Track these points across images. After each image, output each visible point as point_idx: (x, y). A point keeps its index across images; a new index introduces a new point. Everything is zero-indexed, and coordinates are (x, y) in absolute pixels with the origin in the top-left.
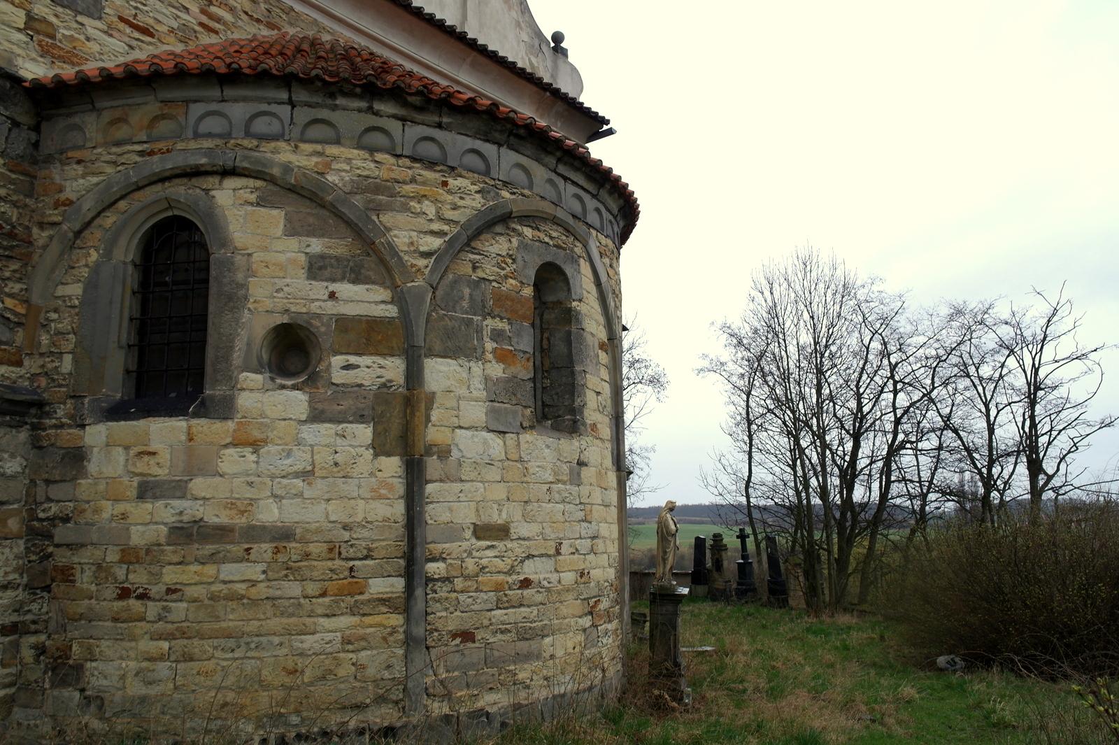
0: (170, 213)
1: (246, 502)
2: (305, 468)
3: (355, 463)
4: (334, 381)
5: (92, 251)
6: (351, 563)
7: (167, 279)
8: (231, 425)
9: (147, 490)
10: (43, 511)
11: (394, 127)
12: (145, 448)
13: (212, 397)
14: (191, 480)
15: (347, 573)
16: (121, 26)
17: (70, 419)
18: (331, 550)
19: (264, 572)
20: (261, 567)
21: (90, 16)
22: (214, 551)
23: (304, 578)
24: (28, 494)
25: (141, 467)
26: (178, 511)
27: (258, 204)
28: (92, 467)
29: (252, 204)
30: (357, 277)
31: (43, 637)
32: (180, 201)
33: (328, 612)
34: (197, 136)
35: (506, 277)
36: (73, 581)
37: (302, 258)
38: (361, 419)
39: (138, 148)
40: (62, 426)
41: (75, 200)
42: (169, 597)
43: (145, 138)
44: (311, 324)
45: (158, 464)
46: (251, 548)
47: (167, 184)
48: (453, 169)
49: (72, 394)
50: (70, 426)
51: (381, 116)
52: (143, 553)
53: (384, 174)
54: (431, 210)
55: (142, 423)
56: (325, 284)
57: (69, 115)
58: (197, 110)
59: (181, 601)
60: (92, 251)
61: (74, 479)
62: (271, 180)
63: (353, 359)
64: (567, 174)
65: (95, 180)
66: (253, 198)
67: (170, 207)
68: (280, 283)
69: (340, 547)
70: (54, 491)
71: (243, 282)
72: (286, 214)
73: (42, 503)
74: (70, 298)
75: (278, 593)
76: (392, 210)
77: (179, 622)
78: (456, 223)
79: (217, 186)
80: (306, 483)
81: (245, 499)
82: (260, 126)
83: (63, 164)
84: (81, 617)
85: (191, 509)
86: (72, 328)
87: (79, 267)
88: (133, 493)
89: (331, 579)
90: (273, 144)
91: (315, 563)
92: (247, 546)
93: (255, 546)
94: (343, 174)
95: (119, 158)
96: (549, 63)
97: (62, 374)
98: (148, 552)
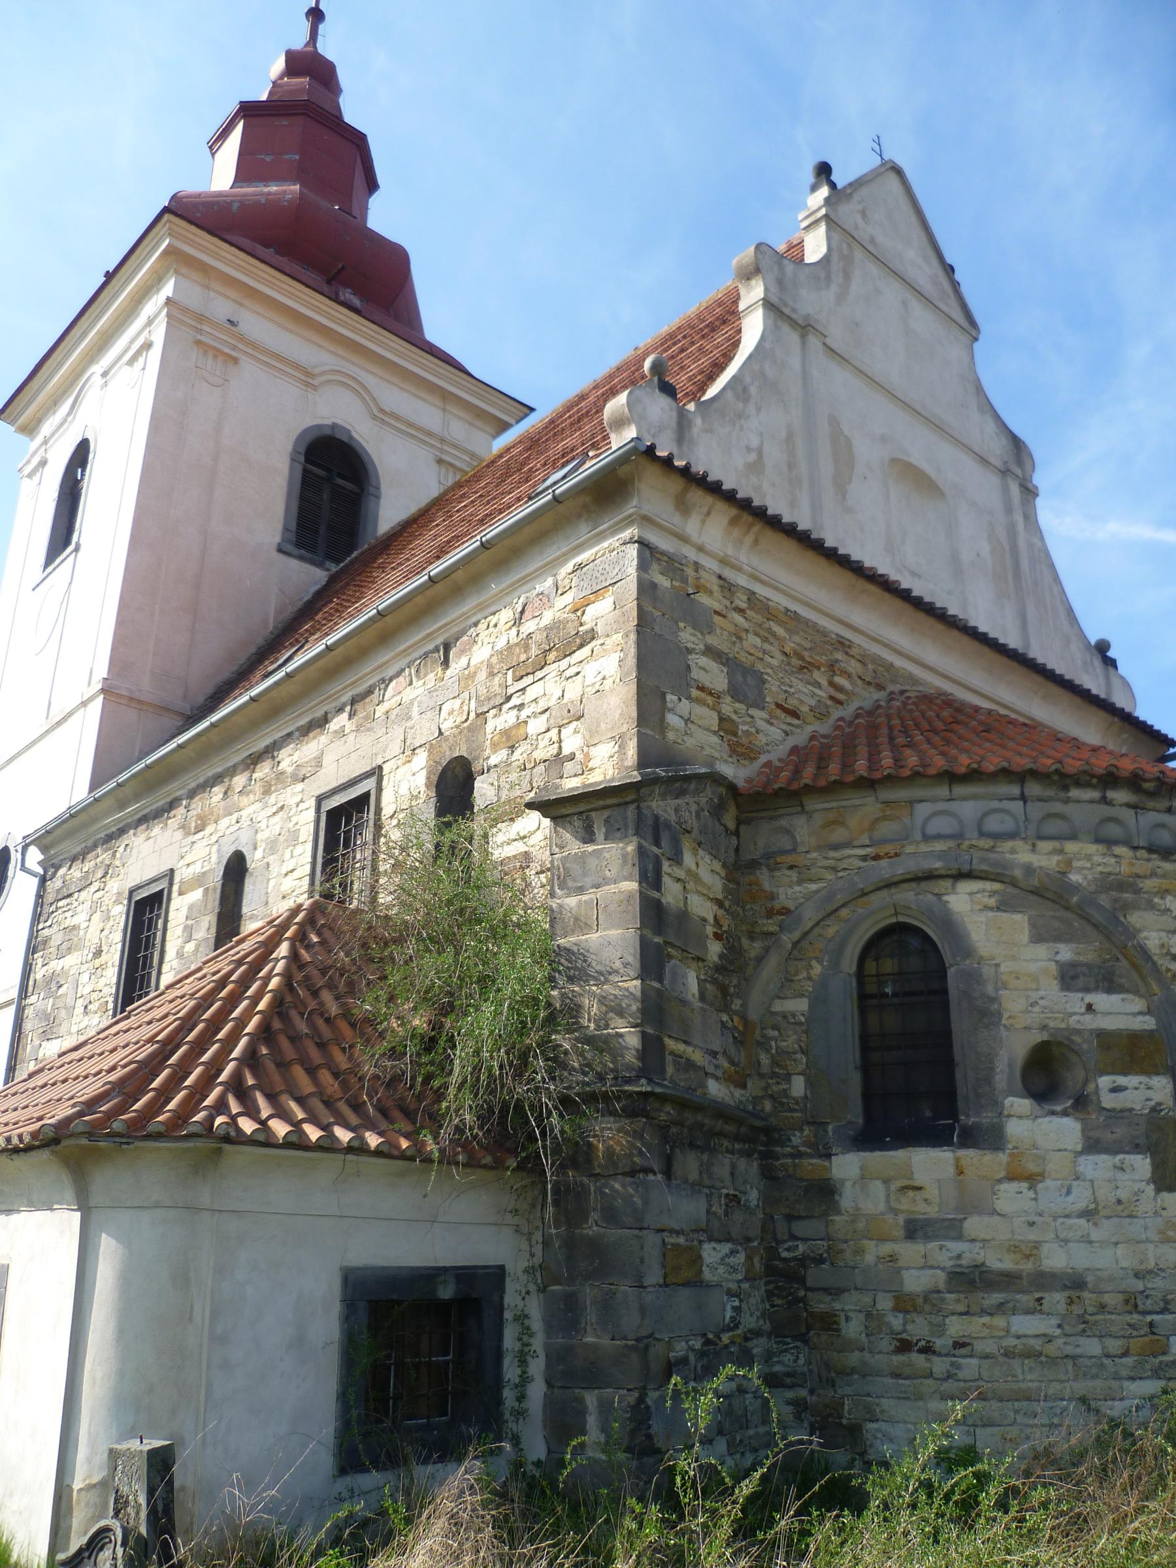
0: (894, 920)
1: (1030, 1245)
2: (1087, 1206)
3: (1138, 1200)
4: (1104, 1105)
5: (814, 963)
6: (1149, 1318)
7: (887, 990)
8: (1003, 1157)
9: (915, 1230)
10: (788, 1250)
11: (1128, 815)
12: (908, 1183)
13: (977, 1126)
14: (965, 1218)
15: (1146, 1329)
16: (778, 712)
17: (809, 1148)
18: (1127, 1302)
19: (1059, 1326)
20: (1054, 1321)
22: (1002, 1301)
23: (1103, 1333)
24: (763, 1230)
25: (905, 1203)
26: (954, 1254)
27: (998, 909)
28: (846, 1201)
29: (991, 909)
30: (1110, 984)
31: (803, 1393)
32: (910, 908)
33: (1132, 1374)
34: (927, 838)
36: (838, 1330)
37: (1053, 967)
38: (1136, 1149)
40: (800, 1155)
41: (792, 909)
42: (957, 1352)
43: (867, 842)
44: (1072, 1042)
45: (926, 1200)
46: (1042, 1298)
47: (893, 890)
49: (811, 1120)
50: (811, 1156)
51: (1114, 805)
52: (920, 1301)
53: (1125, 869)
55: (900, 1154)
56: (1080, 995)
58: (922, 810)
59: (971, 1356)
60: (814, 963)
61: (826, 1214)
62: (1013, 883)
63: (1121, 1080)
66: (992, 902)
67: (896, 914)
68: (1034, 996)
69: (1135, 1298)
70: (800, 1228)
71: (994, 995)
72: (1029, 919)
73: (784, 1241)
74: (793, 1015)
75: (1079, 1351)
76: (1139, 909)
77: (971, 1381)
79: (950, 890)
80: (1090, 1223)
81: (1029, 1242)
82: (993, 824)
83: (771, 869)
84: (853, 1371)
85: (971, 1254)
86: (800, 1046)
87: (799, 981)
88: (900, 1233)
89: (1130, 1336)
91: (1113, 1317)
92: (1037, 1295)
93: (1045, 1295)
94: (1086, 872)
95: (839, 863)
96: (1102, 681)
97: (794, 1098)
98: (926, 1299)
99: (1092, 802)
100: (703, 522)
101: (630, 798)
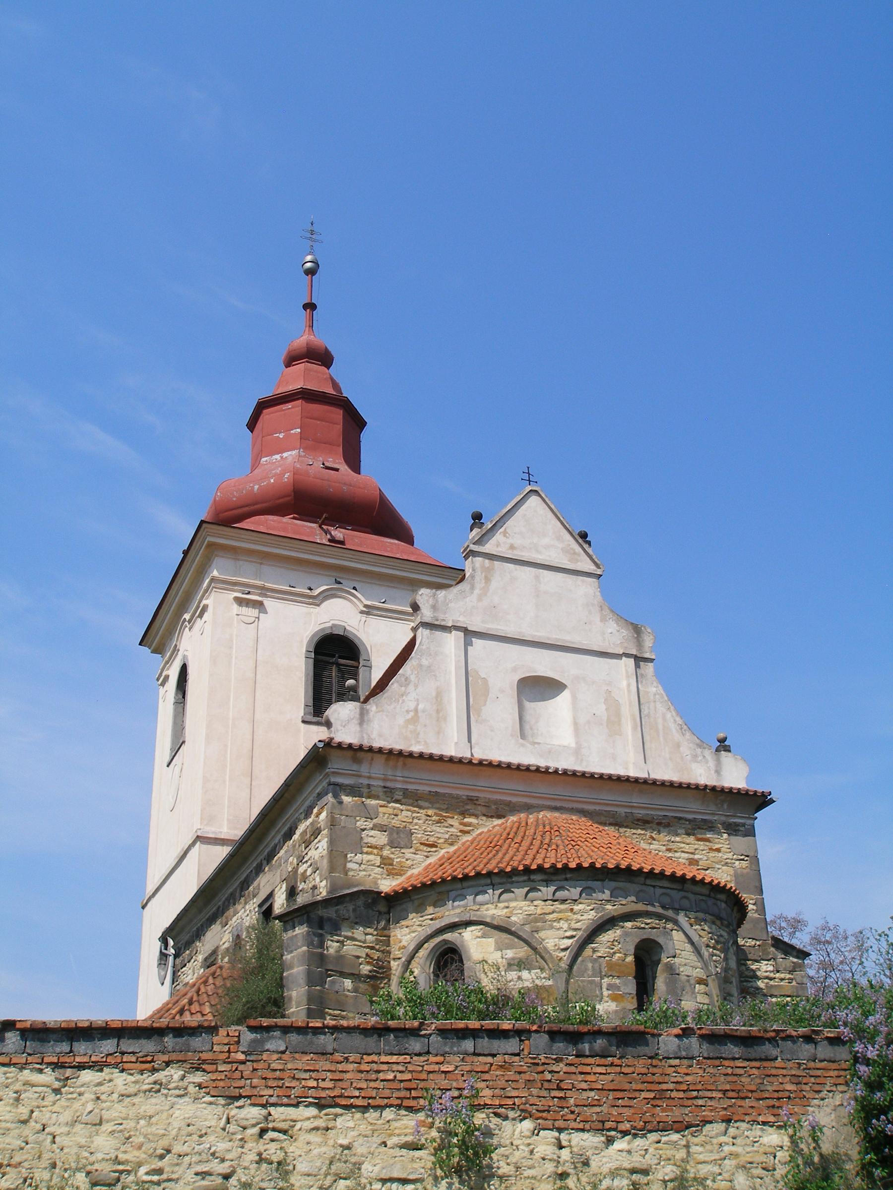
16: (422, 847)
21: (407, 848)
27: (482, 937)
29: (479, 937)
35: (614, 953)
39: (430, 917)
48: (576, 900)
54: (565, 926)
57: (401, 904)
64: (653, 884)
65: (413, 935)
67: (446, 944)
78: (580, 929)
90: (486, 906)
99: (525, 881)
100: (371, 764)
101: (304, 912)
